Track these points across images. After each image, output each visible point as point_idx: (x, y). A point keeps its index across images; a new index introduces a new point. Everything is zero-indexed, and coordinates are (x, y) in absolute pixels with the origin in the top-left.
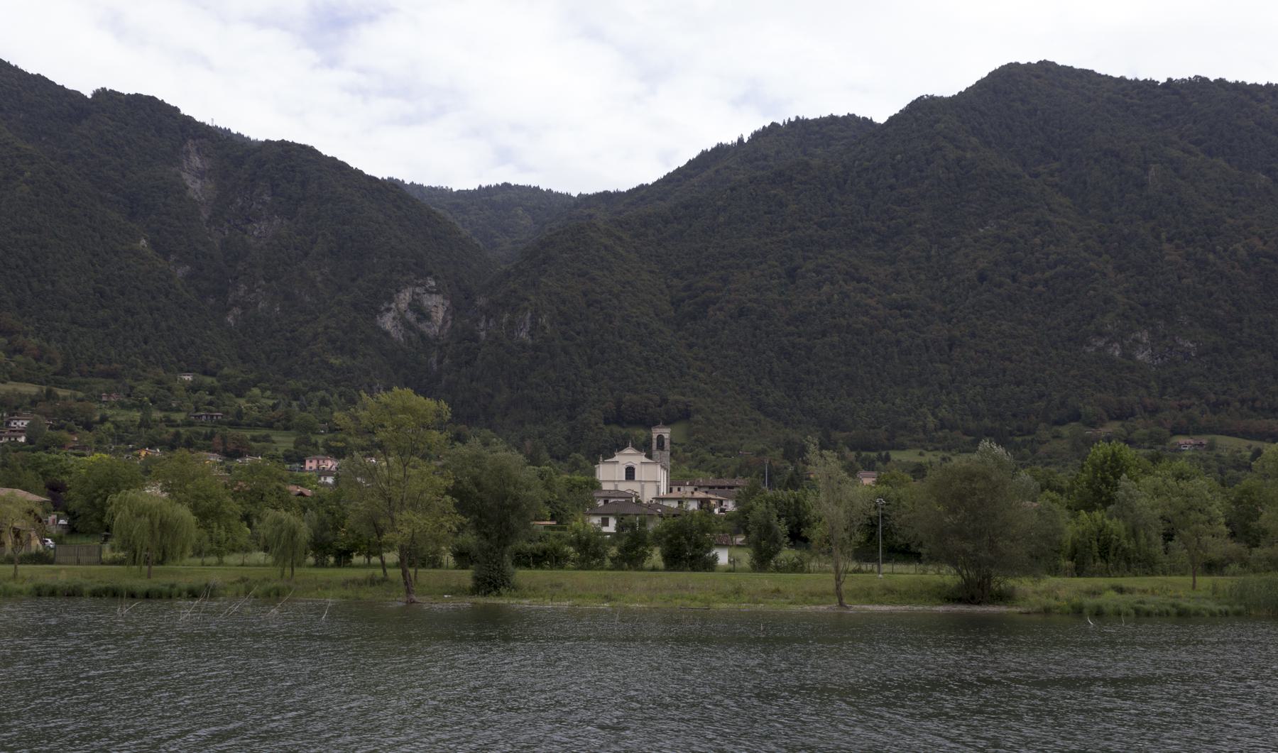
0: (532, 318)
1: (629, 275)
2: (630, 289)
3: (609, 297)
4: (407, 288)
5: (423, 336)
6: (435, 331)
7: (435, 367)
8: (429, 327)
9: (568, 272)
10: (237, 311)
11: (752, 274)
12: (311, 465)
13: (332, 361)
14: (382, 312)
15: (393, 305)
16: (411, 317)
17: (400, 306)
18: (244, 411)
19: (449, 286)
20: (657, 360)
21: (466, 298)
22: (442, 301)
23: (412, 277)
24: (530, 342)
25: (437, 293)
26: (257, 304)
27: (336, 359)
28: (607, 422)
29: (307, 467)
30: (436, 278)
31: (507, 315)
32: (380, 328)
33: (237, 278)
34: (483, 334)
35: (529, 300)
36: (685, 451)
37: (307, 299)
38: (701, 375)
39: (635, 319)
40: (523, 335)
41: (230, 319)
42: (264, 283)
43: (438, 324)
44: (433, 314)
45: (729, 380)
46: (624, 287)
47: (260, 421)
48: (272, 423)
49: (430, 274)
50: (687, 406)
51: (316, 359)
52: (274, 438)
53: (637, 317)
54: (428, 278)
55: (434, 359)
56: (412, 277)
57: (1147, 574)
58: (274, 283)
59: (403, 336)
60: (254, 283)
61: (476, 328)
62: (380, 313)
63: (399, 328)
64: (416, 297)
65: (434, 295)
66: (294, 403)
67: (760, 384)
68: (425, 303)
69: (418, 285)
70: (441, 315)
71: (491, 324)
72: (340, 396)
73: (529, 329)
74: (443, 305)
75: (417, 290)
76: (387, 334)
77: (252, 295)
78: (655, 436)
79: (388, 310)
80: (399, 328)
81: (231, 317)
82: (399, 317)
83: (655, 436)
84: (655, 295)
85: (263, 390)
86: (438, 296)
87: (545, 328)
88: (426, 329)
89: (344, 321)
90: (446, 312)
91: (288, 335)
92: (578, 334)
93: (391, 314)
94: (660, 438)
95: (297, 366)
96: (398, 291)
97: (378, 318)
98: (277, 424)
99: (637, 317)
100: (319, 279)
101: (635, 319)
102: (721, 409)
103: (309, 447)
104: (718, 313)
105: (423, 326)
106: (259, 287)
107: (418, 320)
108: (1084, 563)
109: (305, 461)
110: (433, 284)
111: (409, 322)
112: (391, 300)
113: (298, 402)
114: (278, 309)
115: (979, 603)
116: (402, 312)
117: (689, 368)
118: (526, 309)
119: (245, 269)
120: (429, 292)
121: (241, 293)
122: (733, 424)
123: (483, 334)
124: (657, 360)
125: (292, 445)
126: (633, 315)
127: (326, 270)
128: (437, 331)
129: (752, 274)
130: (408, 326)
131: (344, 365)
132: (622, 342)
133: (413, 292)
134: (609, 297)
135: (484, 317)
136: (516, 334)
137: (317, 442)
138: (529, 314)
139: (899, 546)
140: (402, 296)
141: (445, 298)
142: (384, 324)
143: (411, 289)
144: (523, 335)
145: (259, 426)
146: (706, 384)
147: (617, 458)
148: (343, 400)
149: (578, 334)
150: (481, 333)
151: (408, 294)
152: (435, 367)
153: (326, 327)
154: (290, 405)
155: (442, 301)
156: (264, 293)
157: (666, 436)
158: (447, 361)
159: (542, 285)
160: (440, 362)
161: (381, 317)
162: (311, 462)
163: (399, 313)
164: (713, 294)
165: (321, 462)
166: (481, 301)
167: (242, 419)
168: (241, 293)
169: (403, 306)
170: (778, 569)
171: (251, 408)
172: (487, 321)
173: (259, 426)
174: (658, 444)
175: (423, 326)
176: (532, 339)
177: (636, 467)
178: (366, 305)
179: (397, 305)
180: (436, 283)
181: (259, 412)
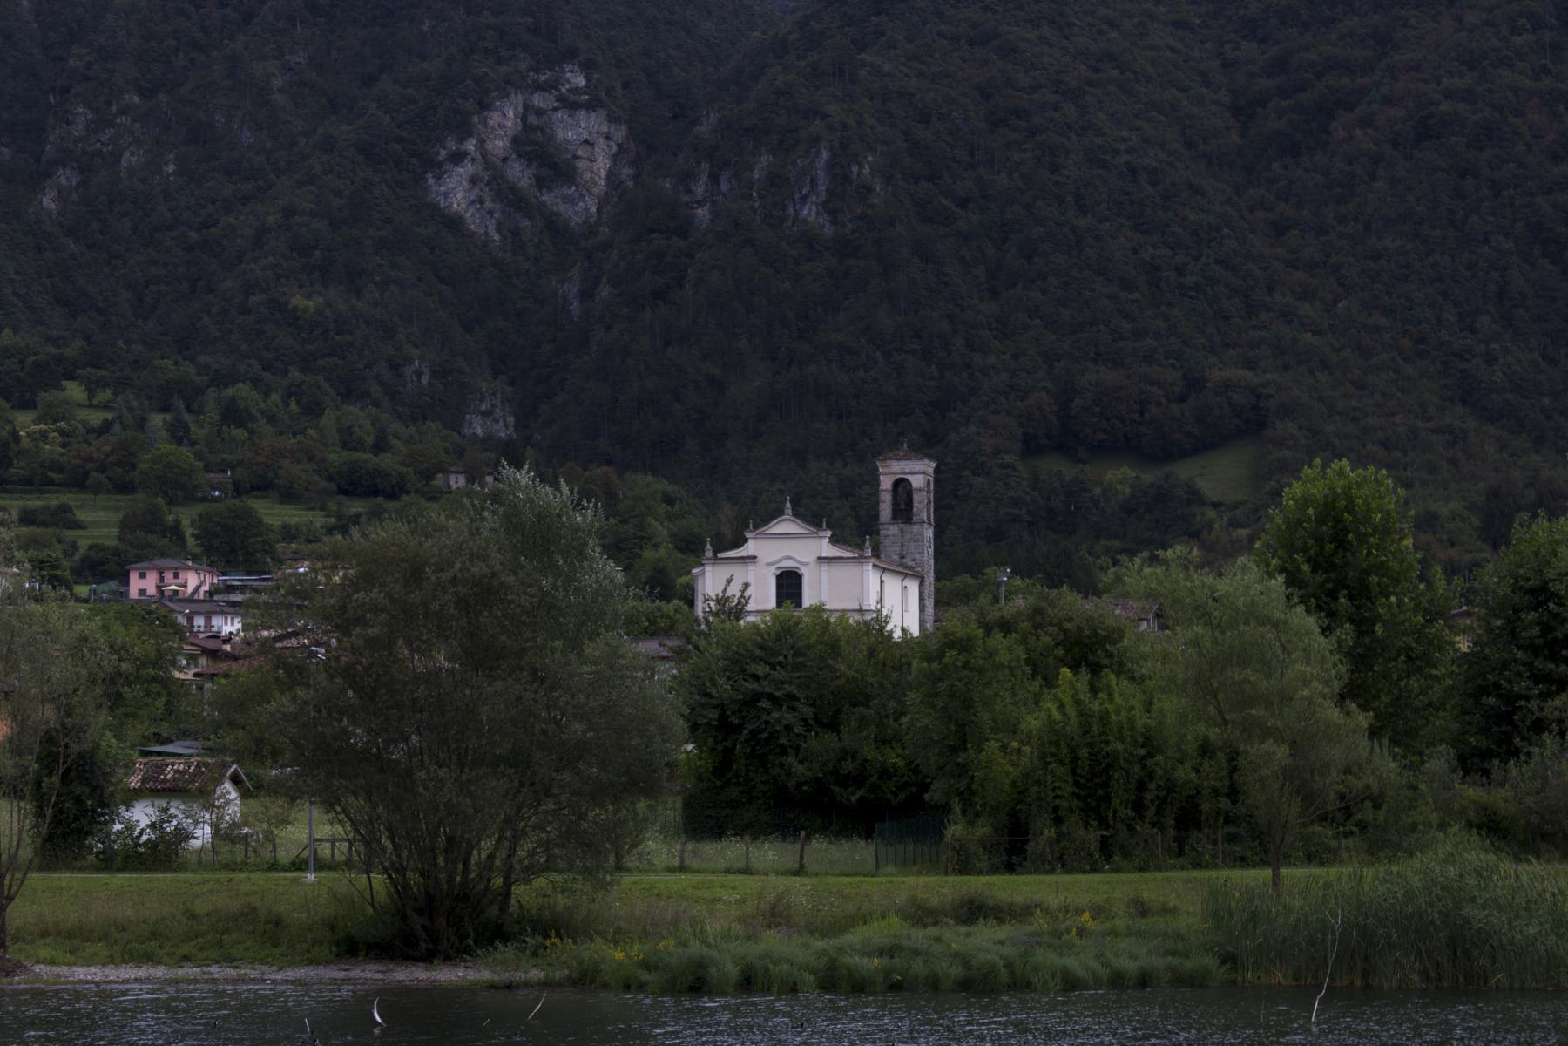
0: (831, 165)
1: (1114, 34)
2: (1115, 73)
3: (1053, 98)
4: (507, 95)
5: (554, 226)
6: (586, 209)
7: (575, 307)
8: (571, 201)
9: (940, 34)
10: (66, 177)
11: (1459, 19)
12: (143, 584)
13: (298, 301)
14: (440, 165)
15: (470, 145)
16: (520, 174)
17: (489, 146)
18: (26, 443)
19: (626, 86)
20: (1180, 271)
21: (675, 117)
22: (605, 128)
23: (523, 66)
24: (828, 230)
25: (591, 106)
26: (117, 156)
27: (309, 297)
28: (1031, 447)
29: (134, 593)
30: (587, 67)
31: (765, 160)
32: (435, 207)
33: (66, 90)
34: (703, 213)
35: (824, 116)
36: (1234, 524)
37: (247, 137)
38: (1306, 309)
39: (1125, 157)
40: (810, 212)
41: (48, 201)
42: (136, 99)
43: (596, 191)
44: (581, 164)
45: (1384, 321)
46: (1097, 70)
47: (61, 470)
48: (86, 474)
49: (571, 54)
50: (1258, 397)
51: (255, 299)
52: (81, 515)
53: (1130, 151)
54: (567, 67)
55: (572, 289)
56: (523, 66)
57: (1243, 859)
58: (163, 98)
59: (499, 229)
60: (109, 103)
61: (686, 199)
62: (431, 164)
63: (488, 205)
64: (532, 120)
65: (582, 114)
66: (157, 420)
67: (1472, 330)
68: (560, 136)
69: (539, 87)
70: (602, 165)
71: (724, 187)
72: (288, 395)
73: (823, 198)
74: (608, 138)
75: (538, 100)
76: (454, 223)
77: (109, 132)
78: (886, 483)
79: (458, 157)
80: (488, 205)
81: (53, 193)
82: (486, 175)
83: (886, 483)
84: (1184, 90)
85: (92, 387)
86: (593, 116)
87: (870, 190)
88: (561, 207)
89: (338, 194)
90: (615, 158)
91: (193, 236)
92: (963, 203)
93: (465, 170)
94: (901, 485)
95: (206, 320)
96: (484, 106)
97: (431, 181)
98: (95, 476)
99: (1130, 151)
100: (278, 82)
101: (1125, 157)
102: (1354, 403)
103: (151, 538)
104: (1358, 132)
105: (552, 199)
106: (123, 112)
107: (541, 183)
108: (702, 832)
109: (127, 576)
110: (580, 81)
111: (513, 189)
112: (463, 129)
113: (168, 417)
114: (171, 168)
115: (427, 958)
116: (498, 162)
117: (1270, 290)
118: (816, 140)
119: (89, 65)
120: (570, 105)
121: (77, 130)
122: (1385, 445)
123: (703, 213)
124: (1180, 271)
125: (115, 531)
126: (1122, 147)
127: (300, 57)
128: (593, 209)
129: (1459, 19)
130: (511, 197)
131: (328, 312)
132: (1083, 222)
133: (526, 107)
134: (1053, 98)
135: (705, 166)
136: (791, 211)
137: (178, 522)
138: (825, 155)
139: (798, 786)
140: (495, 118)
141: (612, 119)
142: (446, 195)
143: (518, 99)
144: (810, 212)
145: (52, 483)
146: (1315, 333)
147: (750, 548)
148: (294, 407)
149: (963, 203)
150: (699, 211)
151: (511, 114)
152: (575, 307)
153: (289, 212)
154: (142, 423)
155: (605, 128)
156: (137, 125)
157: (917, 482)
158: (605, 292)
159: (862, 73)
160: (587, 294)
161: (438, 178)
162: (143, 576)
163: (488, 165)
164: (1346, 81)
165: (169, 576)
166: (707, 125)
167: (10, 465)
168: (77, 130)
169: (498, 145)
170: (108, 861)
171: (44, 435)
172: (714, 178)
173: (52, 483)
174: (895, 504)
175: (552, 199)
176: (834, 222)
177: (803, 570)
178: (397, 147)
179: (481, 142)
180: (588, 79)
181: (64, 445)
